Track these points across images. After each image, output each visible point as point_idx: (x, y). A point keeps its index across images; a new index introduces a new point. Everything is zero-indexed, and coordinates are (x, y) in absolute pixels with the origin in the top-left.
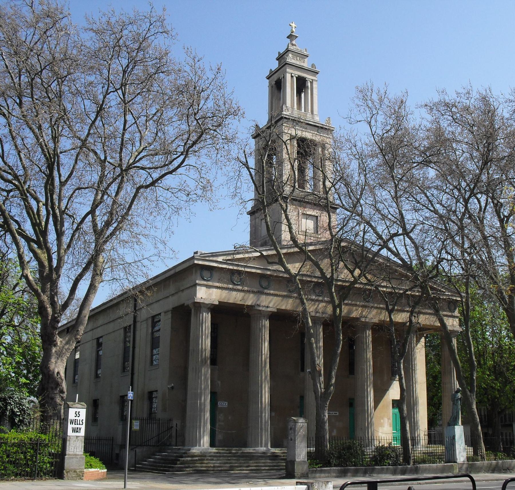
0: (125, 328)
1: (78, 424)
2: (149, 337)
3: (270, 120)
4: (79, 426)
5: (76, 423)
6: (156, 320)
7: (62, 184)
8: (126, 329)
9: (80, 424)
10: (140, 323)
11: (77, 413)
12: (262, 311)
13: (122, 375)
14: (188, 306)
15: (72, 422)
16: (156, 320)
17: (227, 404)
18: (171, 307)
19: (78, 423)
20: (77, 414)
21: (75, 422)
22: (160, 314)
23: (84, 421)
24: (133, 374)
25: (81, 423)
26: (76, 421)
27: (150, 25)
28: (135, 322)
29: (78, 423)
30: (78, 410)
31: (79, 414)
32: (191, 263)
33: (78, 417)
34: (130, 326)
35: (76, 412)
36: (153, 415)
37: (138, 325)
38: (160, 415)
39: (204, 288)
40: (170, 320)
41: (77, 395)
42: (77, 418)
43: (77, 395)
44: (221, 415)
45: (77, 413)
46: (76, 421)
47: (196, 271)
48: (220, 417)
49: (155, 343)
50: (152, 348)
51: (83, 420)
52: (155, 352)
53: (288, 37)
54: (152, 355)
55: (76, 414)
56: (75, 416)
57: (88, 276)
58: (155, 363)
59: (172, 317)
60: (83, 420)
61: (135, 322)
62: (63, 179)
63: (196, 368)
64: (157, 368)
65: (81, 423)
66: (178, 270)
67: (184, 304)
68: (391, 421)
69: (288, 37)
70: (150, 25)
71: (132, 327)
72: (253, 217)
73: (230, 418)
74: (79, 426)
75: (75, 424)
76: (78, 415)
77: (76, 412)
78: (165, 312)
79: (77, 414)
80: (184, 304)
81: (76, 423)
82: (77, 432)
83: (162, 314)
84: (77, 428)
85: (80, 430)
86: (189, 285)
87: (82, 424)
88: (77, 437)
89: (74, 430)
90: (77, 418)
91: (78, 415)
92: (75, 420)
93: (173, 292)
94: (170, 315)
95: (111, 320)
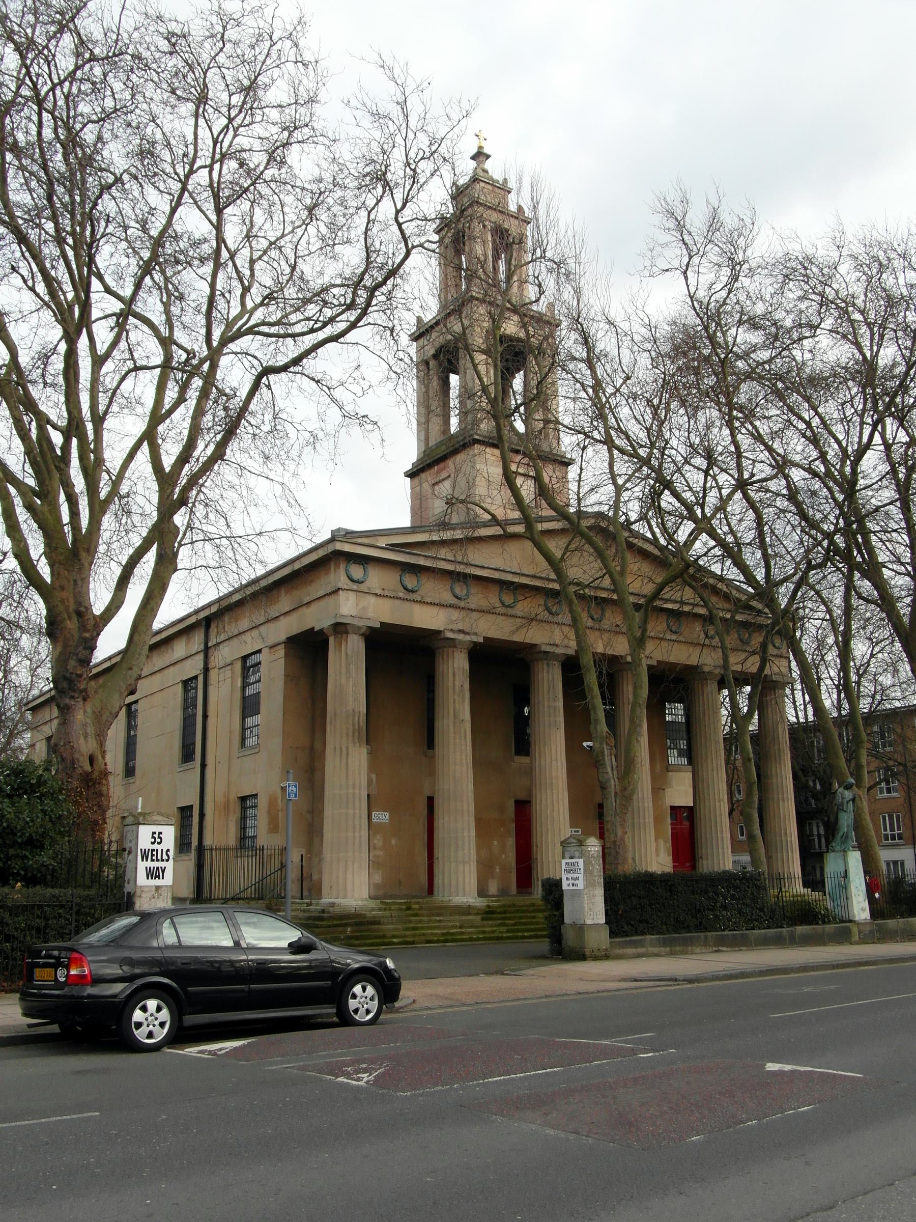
0: (186, 683)
1: (158, 860)
2: (238, 695)
3: (443, 306)
4: (160, 864)
5: (154, 858)
6: (250, 662)
7: (98, 361)
8: (188, 684)
9: (162, 860)
10: (216, 669)
11: (156, 836)
12: (457, 642)
13: (241, 755)
14: (321, 631)
15: (145, 856)
16: (250, 662)
17: (387, 817)
18: (283, 637)
19: (159, 857)
20: (157, 838)
21: (153, 855)
22: (259, 651)
23: (171, 854)
24: (203, 766)
25: (165, 857)
26: (154, 853)
27: (271, 46)
28: (206, 670)
29: (159, 857)
30: (157, 829)
31: (159, 837)
32: (330, 548)
33: (159, 843)
34: (196, 677)
35: (154, 833)
36: (248, 843)
37: (213, 674)
38: (264, 838)
39: (352, 596)
40: (283, 660)
41: (140, 799)
42: (156, 846)
43: (140, 799)
44: (378, 837)
45: (156, 836)
46: (154, 853)
47: (337, 567)
48: (376, 842)
49: (250, 706)
50: (245, 714)
51: (168, 850)
52: (249, 721)
53: (473, 158)
54: (243, 729)
55: (153, 837)
56: (153, 843)
57: (151, 557)
58: (249, 742)
59: (286, 655)
60: (168, 850)
61: (206, 670)
62: (101, 349)
63: (341, 748)
64: (257, 750)
65: (165, 857)
66: (297, 566)
67: (313, 628)
68: (669, 844)
69: (473, 158)
70: (271, 46)
71: (201, 679)
72: (416, 480)
73: (393, 842)
74: (160, 864)
75: (152, 860)
76: (159, 840)
77: (154, 833)
78: (272, 647)
79: (157, 838)
80: (313, 628)
81: (154, 858)
82: (156, 877)
83: (265, 651)
84: (158, 868)
85: (163, 872)
86: (322, 593)
87: (167, 860)
88: (158, 888)
89: (153, 874)
90: (156, 846)
91: (159, 840)
92: (153, 850)
93: (287, 609)
94: (281, 652)
95: (156, 669)
